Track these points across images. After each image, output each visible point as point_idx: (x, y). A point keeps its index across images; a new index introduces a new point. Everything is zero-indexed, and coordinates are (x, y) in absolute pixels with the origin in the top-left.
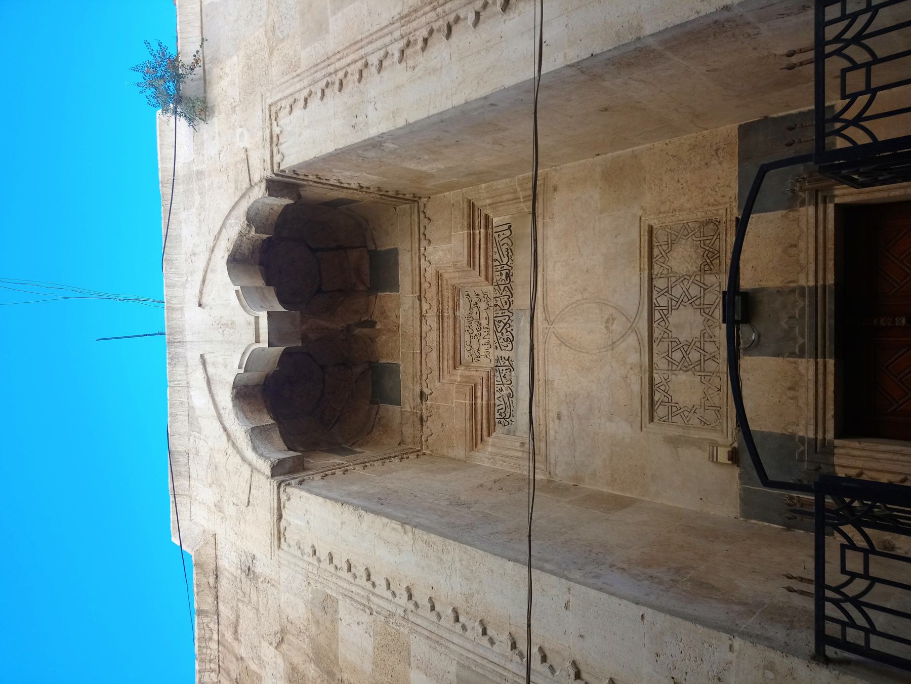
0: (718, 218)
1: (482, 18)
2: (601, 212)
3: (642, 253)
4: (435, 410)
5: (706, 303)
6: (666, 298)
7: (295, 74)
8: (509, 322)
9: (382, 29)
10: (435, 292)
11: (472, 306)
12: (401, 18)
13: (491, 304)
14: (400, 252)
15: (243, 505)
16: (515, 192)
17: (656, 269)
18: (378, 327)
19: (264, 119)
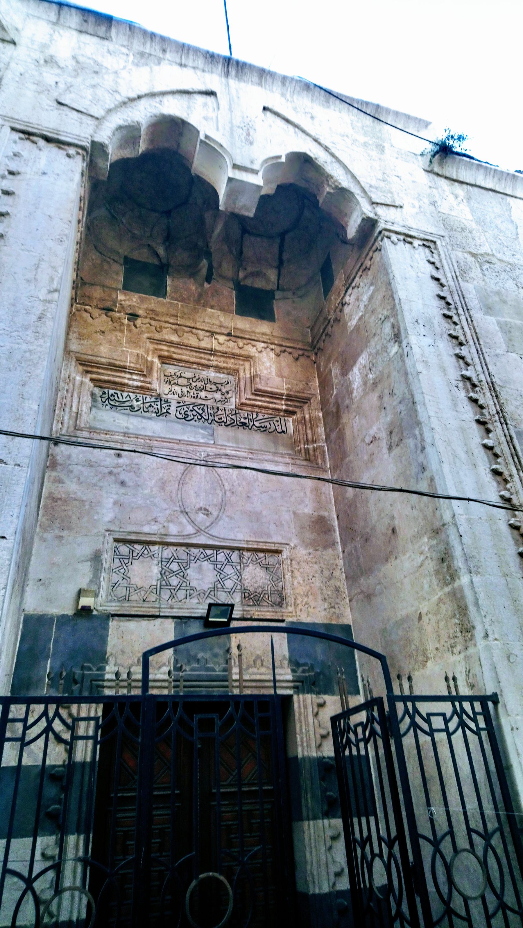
0: (284, 606)
1: (488, 451)
2: (294, 513)
3: (261, 544)
4: (118, 328)
5: (219, 593)
6: (223, 560)
7: (458, 274)
8: (203, 419)
9: (486, 365)
10: (234, 351)
11: (218, 385)
12: (492, 383)
13: (219, 405)
14: (271, 323)
15: (60, 94)
16: (313, 442)
17: (247, 554)
18: (206, 285)
19: (424, 232)
